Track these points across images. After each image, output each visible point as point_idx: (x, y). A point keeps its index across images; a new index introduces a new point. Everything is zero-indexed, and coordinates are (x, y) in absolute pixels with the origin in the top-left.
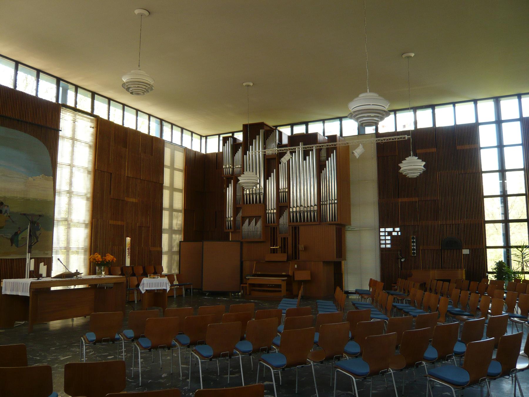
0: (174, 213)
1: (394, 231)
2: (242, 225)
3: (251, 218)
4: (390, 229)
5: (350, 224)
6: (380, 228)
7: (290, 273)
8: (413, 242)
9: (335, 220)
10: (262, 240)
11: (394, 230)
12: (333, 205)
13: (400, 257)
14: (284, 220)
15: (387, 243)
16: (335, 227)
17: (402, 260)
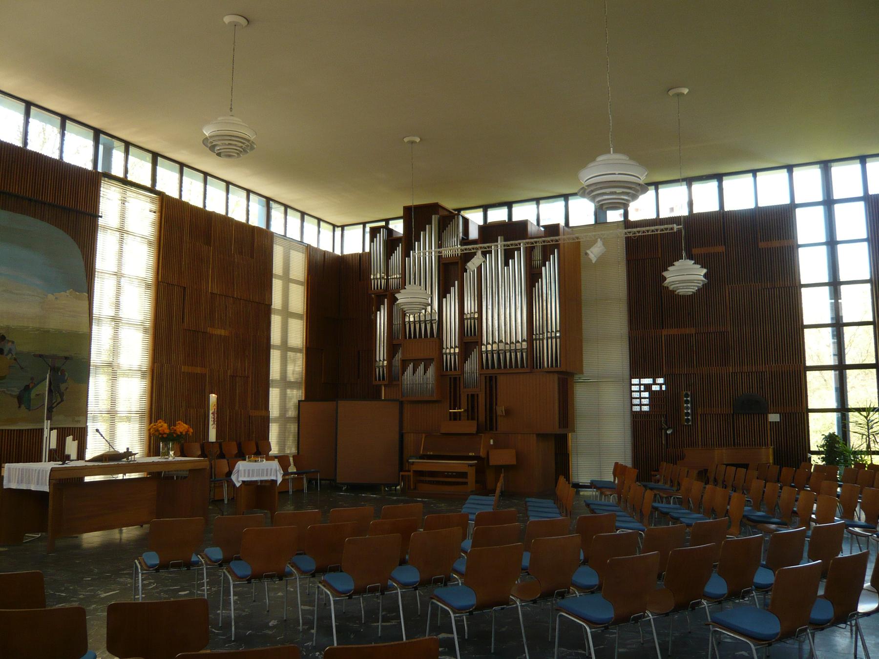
0: (290, 354)
1: (655, 383)
2: (403, 373)
3: (416, 363)
4: (648, 381)
5: (582, 373)
6: (631, 378)
7: (482, 454)
8: (687, 402)
9: (557, 366)
10: (435, 398)
11: (654, 381)
12: (554, 340)
13: (664, 426)
14: (471, 366)
15: (643, 403)
16: (556, 377)
17: (669, 432)
